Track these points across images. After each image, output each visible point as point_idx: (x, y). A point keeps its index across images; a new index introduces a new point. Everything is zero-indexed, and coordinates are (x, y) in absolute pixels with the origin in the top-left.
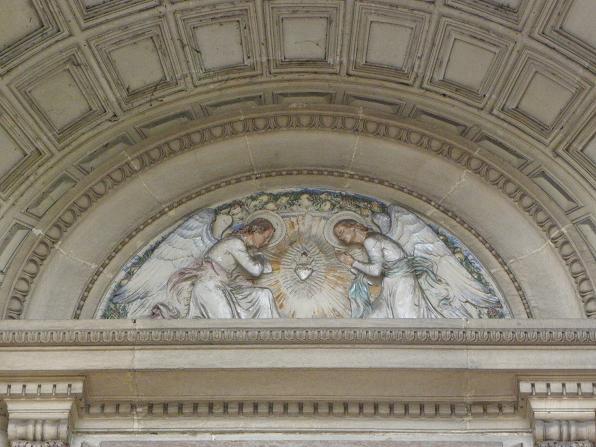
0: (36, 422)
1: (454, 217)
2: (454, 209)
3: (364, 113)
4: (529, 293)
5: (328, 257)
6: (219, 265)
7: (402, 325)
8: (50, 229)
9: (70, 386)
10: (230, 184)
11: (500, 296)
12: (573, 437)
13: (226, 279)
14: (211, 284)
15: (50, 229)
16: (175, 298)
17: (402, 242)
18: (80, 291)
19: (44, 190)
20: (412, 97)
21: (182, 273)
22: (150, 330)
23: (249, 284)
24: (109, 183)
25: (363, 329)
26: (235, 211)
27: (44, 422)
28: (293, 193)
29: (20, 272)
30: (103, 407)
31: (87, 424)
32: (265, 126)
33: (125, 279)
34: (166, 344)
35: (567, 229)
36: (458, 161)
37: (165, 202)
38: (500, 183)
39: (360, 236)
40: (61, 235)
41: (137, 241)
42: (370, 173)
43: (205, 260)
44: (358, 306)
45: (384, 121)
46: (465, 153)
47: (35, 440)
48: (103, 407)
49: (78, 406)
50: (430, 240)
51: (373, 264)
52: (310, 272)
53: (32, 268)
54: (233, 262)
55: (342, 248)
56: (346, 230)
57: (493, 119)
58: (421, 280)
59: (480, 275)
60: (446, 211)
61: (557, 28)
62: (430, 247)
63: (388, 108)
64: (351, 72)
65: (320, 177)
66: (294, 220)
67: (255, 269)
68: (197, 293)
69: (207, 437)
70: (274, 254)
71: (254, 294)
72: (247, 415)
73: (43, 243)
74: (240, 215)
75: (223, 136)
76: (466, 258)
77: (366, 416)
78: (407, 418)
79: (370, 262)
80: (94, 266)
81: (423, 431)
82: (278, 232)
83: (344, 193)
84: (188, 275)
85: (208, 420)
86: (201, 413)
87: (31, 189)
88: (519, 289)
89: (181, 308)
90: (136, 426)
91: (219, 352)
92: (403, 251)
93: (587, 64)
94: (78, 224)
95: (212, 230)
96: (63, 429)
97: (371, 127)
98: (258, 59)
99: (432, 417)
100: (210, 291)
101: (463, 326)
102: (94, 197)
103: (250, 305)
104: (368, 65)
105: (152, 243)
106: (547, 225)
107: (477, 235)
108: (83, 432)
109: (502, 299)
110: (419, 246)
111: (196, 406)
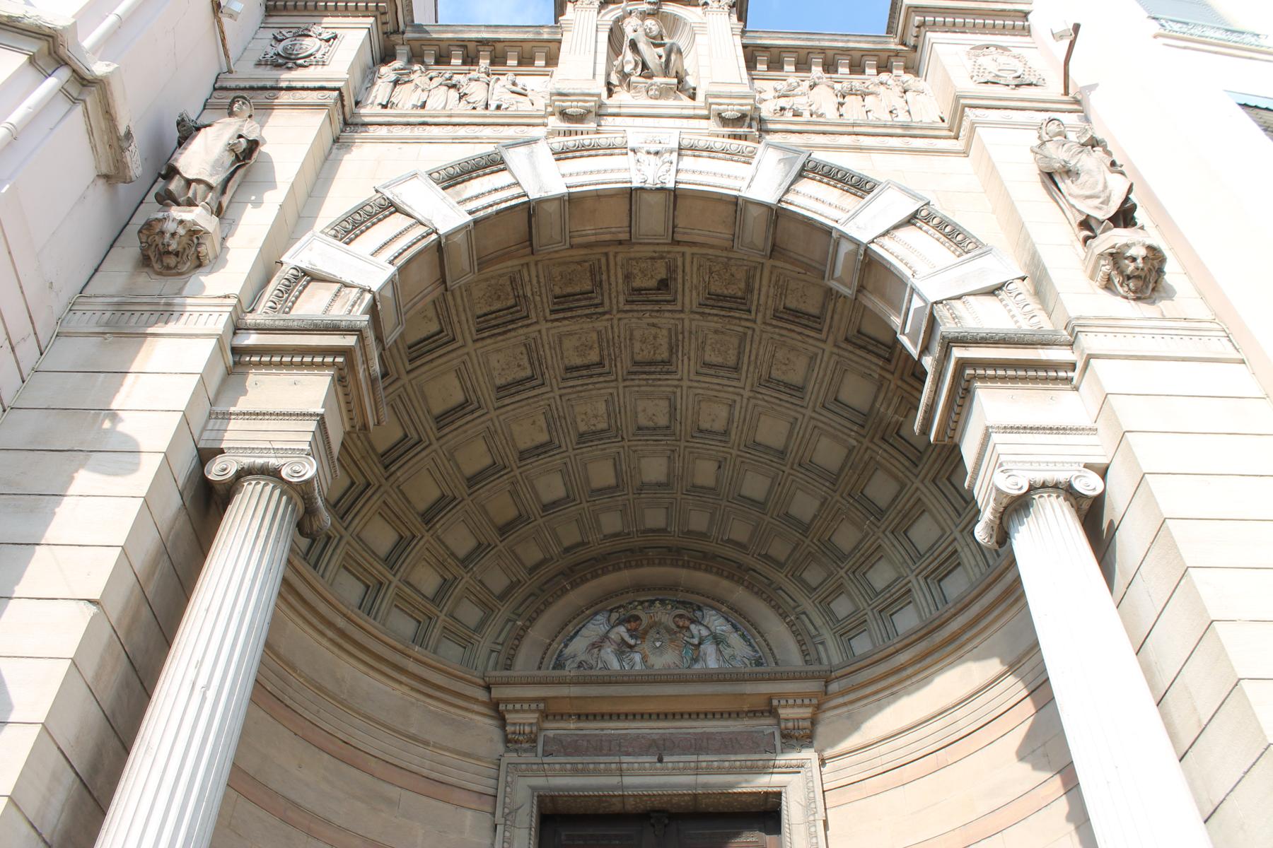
0: (520, 724)
1: (736, 612)
4: (776, 651)
14: (609, 650)
17: (709, 626)
23: (629, 650)
27: (524, 724)
30: (555, 716)
31: (547, 725)
38: (759, 594)
39: (687, 623)
41: (570, 627)
43: (605, 637)
47: (520, 733)
48: (555, 716)
55: (678, 630)
57: (754, 559)
58: (720, 646)
60: (732, 609)
62: (724, 628)
67: (632, 642)
72: (630, 720)
73: (522, 629)
79: (693, 637)
80: (548, 641)
84: (597, 645)
89: (594, 663)
90: (572, 726)
96: (534, 729)
97: (692, 564)
102: (547, 604)
104: (689, 532)
105: (578, 628)
107: (748, 621)
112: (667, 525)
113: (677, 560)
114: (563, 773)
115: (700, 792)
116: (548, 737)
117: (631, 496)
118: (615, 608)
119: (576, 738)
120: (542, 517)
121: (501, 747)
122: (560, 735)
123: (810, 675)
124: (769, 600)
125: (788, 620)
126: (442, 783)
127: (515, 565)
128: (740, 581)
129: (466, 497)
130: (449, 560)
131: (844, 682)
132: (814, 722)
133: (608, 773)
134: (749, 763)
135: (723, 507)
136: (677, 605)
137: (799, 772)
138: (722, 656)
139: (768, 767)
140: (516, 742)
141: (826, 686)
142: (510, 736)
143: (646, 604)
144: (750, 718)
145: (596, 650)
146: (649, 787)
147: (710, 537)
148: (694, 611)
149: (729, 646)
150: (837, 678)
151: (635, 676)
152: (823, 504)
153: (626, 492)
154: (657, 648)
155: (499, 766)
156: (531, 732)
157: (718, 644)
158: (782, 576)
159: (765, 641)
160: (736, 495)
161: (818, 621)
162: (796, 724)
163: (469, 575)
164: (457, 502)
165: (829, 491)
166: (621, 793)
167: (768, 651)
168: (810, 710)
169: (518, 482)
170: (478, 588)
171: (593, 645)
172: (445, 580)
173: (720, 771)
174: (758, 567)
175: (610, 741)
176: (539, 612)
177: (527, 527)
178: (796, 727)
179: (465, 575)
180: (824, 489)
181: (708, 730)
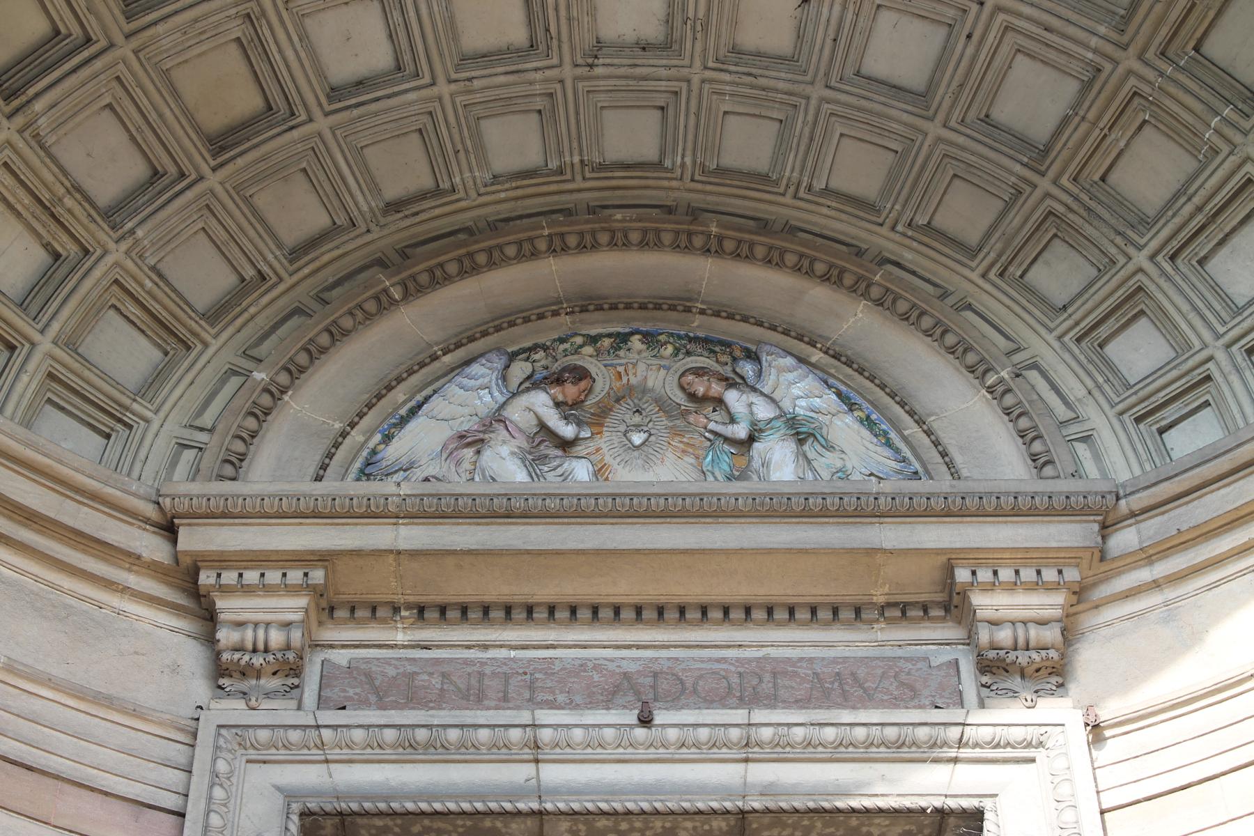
0: (256, 625)
1: (849, 363)
2: (849, 353)
3: (717, 227)
5: (670, 417)
6: (517, 426)
7: (786, 490)
8: (277, 374)
9: (306, 575)
10: (530, 321)
11: (917, 466)
12: (1032, 644)
13: (525, 445)
14: (505, 450)
15: (277, 374)
16: (454, 470)
17: (776, 396)
18: (318, 458)
20: (782, 208)
21: (462, 437)
22: (421, 497)
23: (559, 453)
24: (360, 315)
25: (730, 495)
26: (537, 357)
27: (268, 625)
28: (619, 334)
30: (353, 610)
31: (330, 634)
32: (579, 245)
33: (380, 443)
34: (444, 516)
36: (852, 289)
37: (437, 344)
38: (911, 318)
39: (716, 388)
40: (292, 382)
41: (399, 394)
42: (729, 307)
43: (497, 418)
45: (746, 236)
46: (860, 278)
47: (255, 651)
48: (353, 610)
49: (317, 605)
50: (817, 392)
51: (738, 423)
52: (646, 435)
53: (251, 423)
54: (535, 422)
55: (691, 406)
57: (897, 237)
58: (806, 447)
59: (888, 439)
60: (836, 356)
62: (817, 402)
63: (751, 223)
64: (697, 177)
65: (658, 314)
66: (621, 369)
67: (568, 431)
68: (483, 463)
69: (503, 653)
70: (592, 414)
71: (566, 465)
72: (561, 623)
73: (266, 390)
74: (543, 362)
75: (520, 257)
76: (868, 417)
78: (793, 625)
79: (733, 420)
80: (338, 425)
83: (691, 335)
84: (473, 440)
86: (494, 618)
88: (944, 454)
90: (401, 637)
92: (780, 408)
93: (1026, 160)
95: (504, 378)
96: (296, 636)
97: (729, 245)
98: (568, 159)
99: (827, 624)
101: (874, 490)
102: (338, 334)
104: (722, 171)
105: (419, 397)
107: (882, 387)
108: (323, 646)
109: (920, 470)
110: (803, 403)
111: (486, 610)
112: (663, 153)
113: (690, 234)
114: (375, 753)
115: (757, 805)
117: (567, 72)
118: (524, 350)
119: (410, 668)
120: (327, 114)
121: (200, 689)
122: (367, 661)
123: (1058, 503)
124: (937, 333)
126: (30, 768)
127: (252, 233)
128: (860, 289)
129: (119, 38)
130: (68, 202)
131: (1154, 528)
132: (1070, 634)
133: (500, 752)
134: (891, 733)
135: (813, 102)
137: (1033, 760)
139: (945, 744)
140: (245, 672)
141: (1104, 538)
142: (226, 656)
144: (891, 621)
145: (469, 453)
146: (614, 791)
147: (777, 183)
148: (735, 359)
149: (829, 447)
150: (1133, 515)
151: (579, 497)
152: (1086, 86)
153: (555, 61)
154: (638, 447)
155: (195, 735)
156: (288, 647)
157: (801, 442)
158: (975, 276)
160: (849, 72)
161: (1074, 387)
163: (124, 246)
164: (93, 50)
165: (1109, 49)
166: (535, 806)
168: (1059, 598)
169: (263, 13)
170: (149, 284)
171: (462, 438)
172: (57, 256)
173: (811, 752)
174: (908, 257)
175: (507, 678)
176: (315, 352)
177: (288, 137)
179: (111, 245)
180: (1094, 42)
181: (774, 652)
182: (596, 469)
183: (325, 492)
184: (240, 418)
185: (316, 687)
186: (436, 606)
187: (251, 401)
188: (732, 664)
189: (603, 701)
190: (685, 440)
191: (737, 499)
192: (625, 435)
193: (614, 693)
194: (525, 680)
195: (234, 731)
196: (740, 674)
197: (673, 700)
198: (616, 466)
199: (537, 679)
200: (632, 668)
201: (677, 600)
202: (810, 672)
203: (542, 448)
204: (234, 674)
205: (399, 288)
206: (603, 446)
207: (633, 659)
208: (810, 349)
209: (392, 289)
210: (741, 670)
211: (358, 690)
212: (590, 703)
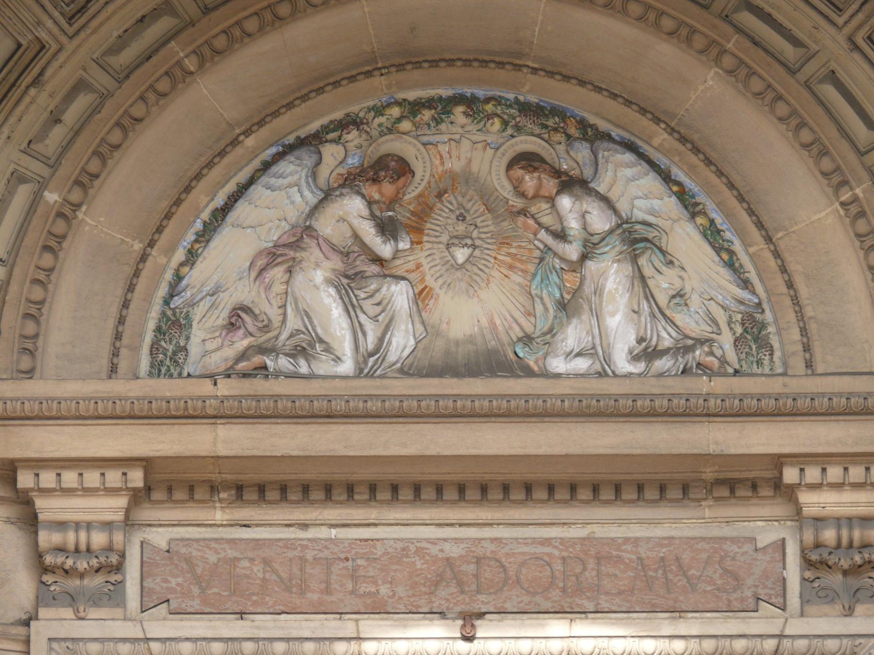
0: (77, 526)
1: (696, 150)
4: (804, 292)
5: (497, 219)
12: (856, 543)
16: (264, 296)
17: (613, 195)
19: (51, 107)
22: (239, 398)
24: (151, 97)
25: (556, 396)
26: (349, 137)
27: (89, 526)
29: (32, 267)
35: (864, 192)
44: (546, 309)
47: (77, 550)
48: (170, 490)
51: (571, 242)
54: (349, 234)
55: (518, 203)
56: (527, 178)
60: (683, 140)
61: (808, 84)
62: (656, 203)
67: (385, 250)
71: (384, 289)
73: (60, 215)
74: (356, 142)
77: (558, 502)
80: (138, 246)
81: (641, 522)
82: (418, 177)
85: (325, 508)
87: (33, 107)
88: (790, 285)
89: (274, 313)
90: (219, 516)
91: (343, 427)
94: (109, 173)
100: (317, 287)
103: (378, 309)
106: (836, 179)
107: (731, 186)
116: (155, 549)
119: (231, 553)
122: (187, 541)
125: (846, 196)
136: (521, 120)
138: (649, 296)
143: (427, 115)
154: (461, 267)
156: (110, 548)
159: (777, 254)
162: (845, 533)
167: (784, 289)
175: (328, 563)
178: (845, 541)
182: (417, 291)
183: (141, 394)
184: (36, 256)
185: (137, 575)
186: (254, 485)
187: (45, 231)
188: (555, 547)
189: (425, 593)
190: (513, 251)
191: (563, 401)
192: (447, 249)
193: (437, 584)
194: (346, 568)
195: (64, 645)
196: (564, 559)
197: (495, 593)
198: (437, 290)
199: (359, 566)
200: (454, 551)
201: (500, 478)
202: (634, 557)
203: (358, 263)
204: (57, 571)
205: (194, 58)
206: (424, 261)
207: (457, 541)
208: (653, 127)
209: (186, 60)
210: (564, 554)
211: (180, 580)
212: (413, 595)
